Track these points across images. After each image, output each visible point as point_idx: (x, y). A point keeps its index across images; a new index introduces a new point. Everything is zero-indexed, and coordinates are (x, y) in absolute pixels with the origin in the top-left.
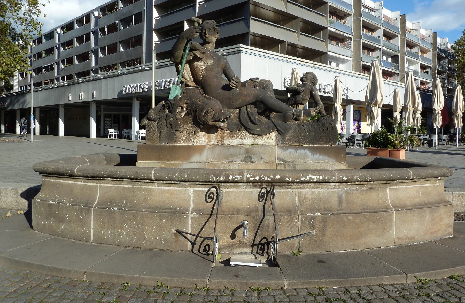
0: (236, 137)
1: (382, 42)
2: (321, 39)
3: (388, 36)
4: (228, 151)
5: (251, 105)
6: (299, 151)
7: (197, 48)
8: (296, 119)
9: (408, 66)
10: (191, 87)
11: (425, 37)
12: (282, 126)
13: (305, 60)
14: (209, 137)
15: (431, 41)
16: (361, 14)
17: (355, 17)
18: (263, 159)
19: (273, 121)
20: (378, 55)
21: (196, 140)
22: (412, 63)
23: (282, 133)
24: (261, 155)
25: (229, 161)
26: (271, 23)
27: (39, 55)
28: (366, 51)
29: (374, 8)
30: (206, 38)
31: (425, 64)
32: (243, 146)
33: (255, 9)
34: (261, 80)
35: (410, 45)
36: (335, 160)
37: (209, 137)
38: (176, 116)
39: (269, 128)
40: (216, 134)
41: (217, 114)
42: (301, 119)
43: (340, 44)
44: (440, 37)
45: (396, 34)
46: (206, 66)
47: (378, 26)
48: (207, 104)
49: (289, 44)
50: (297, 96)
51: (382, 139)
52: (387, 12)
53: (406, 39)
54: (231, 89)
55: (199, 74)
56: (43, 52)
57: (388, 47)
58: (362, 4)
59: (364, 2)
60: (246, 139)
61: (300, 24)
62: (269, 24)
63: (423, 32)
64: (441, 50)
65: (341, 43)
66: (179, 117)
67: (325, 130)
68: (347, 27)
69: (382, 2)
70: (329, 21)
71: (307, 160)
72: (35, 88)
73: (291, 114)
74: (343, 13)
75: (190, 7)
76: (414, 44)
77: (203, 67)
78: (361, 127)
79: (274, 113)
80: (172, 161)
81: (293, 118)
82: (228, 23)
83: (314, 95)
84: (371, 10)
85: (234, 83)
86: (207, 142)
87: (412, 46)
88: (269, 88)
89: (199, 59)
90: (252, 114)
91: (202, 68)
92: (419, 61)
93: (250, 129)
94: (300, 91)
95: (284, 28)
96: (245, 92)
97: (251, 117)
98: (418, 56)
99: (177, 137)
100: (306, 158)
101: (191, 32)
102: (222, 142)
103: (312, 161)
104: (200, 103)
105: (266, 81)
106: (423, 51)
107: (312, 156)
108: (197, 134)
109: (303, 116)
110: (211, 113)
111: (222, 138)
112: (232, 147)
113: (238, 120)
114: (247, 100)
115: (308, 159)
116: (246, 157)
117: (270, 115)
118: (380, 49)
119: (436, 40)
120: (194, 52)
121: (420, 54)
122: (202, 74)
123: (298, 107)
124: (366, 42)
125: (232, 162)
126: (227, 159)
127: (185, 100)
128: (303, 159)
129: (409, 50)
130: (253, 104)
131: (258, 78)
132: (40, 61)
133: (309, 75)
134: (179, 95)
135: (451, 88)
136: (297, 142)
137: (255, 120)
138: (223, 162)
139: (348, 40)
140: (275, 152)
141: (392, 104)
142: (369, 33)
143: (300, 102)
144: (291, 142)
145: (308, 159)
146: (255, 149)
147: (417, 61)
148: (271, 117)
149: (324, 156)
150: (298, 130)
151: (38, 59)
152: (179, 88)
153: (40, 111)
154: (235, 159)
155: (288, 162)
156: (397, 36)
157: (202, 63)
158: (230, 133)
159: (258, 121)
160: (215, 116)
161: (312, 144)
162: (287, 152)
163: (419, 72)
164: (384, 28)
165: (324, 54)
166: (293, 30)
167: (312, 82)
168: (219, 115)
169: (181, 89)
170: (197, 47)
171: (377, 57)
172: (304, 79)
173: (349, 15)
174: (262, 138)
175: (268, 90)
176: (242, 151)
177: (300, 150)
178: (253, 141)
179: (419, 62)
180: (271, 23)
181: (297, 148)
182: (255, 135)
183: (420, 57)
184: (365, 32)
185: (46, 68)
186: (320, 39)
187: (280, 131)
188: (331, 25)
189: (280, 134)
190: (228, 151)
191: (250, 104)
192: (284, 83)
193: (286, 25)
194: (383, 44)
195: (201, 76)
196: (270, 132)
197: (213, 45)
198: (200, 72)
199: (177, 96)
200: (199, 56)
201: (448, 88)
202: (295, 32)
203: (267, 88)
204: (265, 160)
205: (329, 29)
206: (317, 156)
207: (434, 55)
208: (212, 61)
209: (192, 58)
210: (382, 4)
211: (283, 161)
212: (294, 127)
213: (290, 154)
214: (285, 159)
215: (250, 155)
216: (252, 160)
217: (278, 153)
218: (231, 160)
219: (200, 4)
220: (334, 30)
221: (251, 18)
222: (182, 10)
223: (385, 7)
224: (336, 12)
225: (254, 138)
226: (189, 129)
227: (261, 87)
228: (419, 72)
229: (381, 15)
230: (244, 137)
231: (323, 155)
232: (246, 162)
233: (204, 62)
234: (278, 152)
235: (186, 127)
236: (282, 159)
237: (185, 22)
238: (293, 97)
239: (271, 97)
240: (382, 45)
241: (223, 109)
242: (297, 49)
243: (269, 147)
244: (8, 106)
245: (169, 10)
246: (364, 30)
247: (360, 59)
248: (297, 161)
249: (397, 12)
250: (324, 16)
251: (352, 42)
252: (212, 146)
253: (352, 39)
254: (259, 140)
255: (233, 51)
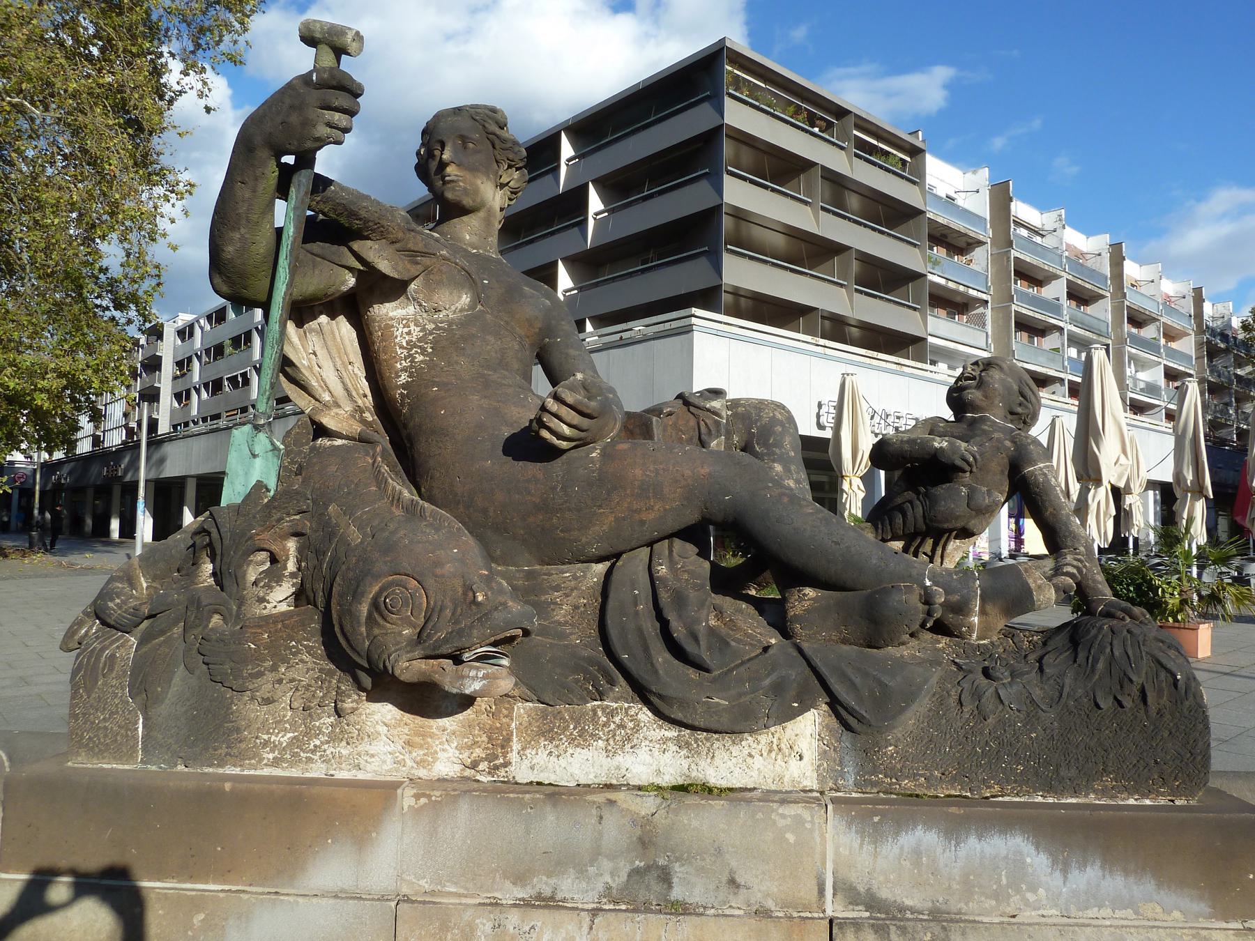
0: (583, 738)
1: (1065, 312)
2: (910, 304)
3: (1079, 296)
4: (528, 832)
5: (678, 544)
6: (973, 841)
7: (366, 221)
8: (941, 628)
9: (1133, 372)
10: (339, 442)
11: (1173, 299)
12: (858, 681)
13: (874, 354)
14: (418, 734)
15: (1190, 310)
16: (1011, 242)
17: (995, 248)
18: (743, 891)
19: (805, 646)
20: (1057, 345)
21: (344, 752)
22: (1143, 366)
23: (860, 719)
24: (734, 864)
25: (533, 893)
26: (779, 262)
27: (219, 351)
28: (1025, 335)
29: (1040, 227)
30: (445, 183)
31: (1175, 366)
32: (619, 796)
33: (737, 228)
34: (735, 404)
35: (1138, 320)
36: (1203, 907)
37: (424, 736)
38: (241, 602)
39: (778, 689)
40: (460, 716)
41: (448, 612)
42: (970, 628)
43: (957, 317)
44: (1210, 300)
45: (1101, 292)
46: (430, 326)
47: (1054, 271)
48: (389, 548)
49: (825, 315)
50: (940, 490)
51: (1132, 589)
52: (1074, 238)
53: (1126, 303)
54: (551, 453)
55: (392, 367)
56: (228, 342)
57: (1082, 323)
58: (1012, 218)
59: (1016, 212)
60: (643, 753)
61: (855, 266)
62: (774, 265)
63: (1169, 287)
64: (1213, 332)
65: (961, 313)
66: (258, 611)
67: (1127, 703)
68: (976, 273)
69: (1063, 211)
70: (930, 258)
71: (1027, 903)
72: (206, 424)
73: (914, 600)
74: (964, 239)
75: (573, 225)
76: (1145, 317)
77: (416, 332)
78: (1023, 533)
79: (810, 592)
80: (191, 878)
81: (923, 626)
82: (667, 264)
83: (1037, 484)
84: (1036, 232)
85: (568, 419)
86: (409, 763)
87: (1140, 321)
88: (778, 444)
89: (395, 289)
90: (680, 600)
91: (409, 333)
92: (1160, 360)
93: (660, 697)
94: (959, 462)
95: (812, 276)
96: (638, 472)
97: (671, 616)
98: (1159, 347)
99: (238, 730)
100: (1018, 891)
101: (292, 107)
102: (497, 768)
103: (1056, 906)
104: (355, 536)
105: (761, 405)
106: (1171, 335)
107: (1058, 874)
108: (352, 718)
109: (983, 612)
110: (405, 604)
111: (499, 743)
112: (548, 808)
113: (594, 632)
114: (650, 516)
115: (1031, 897)
116: (636, 872)
117: (784, 600)
118: (1061, 329)
119: (1203, 307)
120: (356, 245)
121: (1163, 341)
122: (404, 370)
123: (939, 552)
124: (1024, 311)
125: (552, 898)
126: (520, 879)
127: (288, 514)
128: (999, 896)
129: (1134, 331)
130: (693, 534)
131: (717, 393)
132: (221, 363)
133: (995, 374)
134: (272, 483)
135: (1245, 427)
136: (954, 779)
137: (695, 637)
138: (496, 904)
139: (978, 307)
140: (818, 849)
141: (1172, 481)
142: (1031, 290)
143: (959, 524)
144: (914, 777)
145: (1031, 897)
146: (695, 823)
147: (1156, 359)
148: (791, 613)
149: (1131, 879)
150: (960, 703)
151: (215, 359)
152: (270, 447)
153: (198, 485)
154: (568, 886)
155: (902, 909)
156: (1103, 297)
157: (411, 310)
158: (544, 716)
159: (709, 648)
160: (430, 624)
161: (1049, 789)
162: (896, 850)
163: (1163, 387)
164: (1070, 278)
165: (917, 341)
166: (835, 280)
167: (1012, 413)
168: (457, 622)
169: (275, 448)
170: (363, 213)
171: (1054, 349)
172: (973, 395)
173: (980, 243)
174: (735, 750)
175: (774, 453)
176: (614, 831)
177: (980, 837)
178: (685, 763)
179: (1160, 363)
180: (779, 262)
181: (954, 830)
182: (693, 728)
183: (1162, 350)
184: (1020, 286)
185: (233, 380)
186: (907, 303)
187: (851, 712)
188: (933, 269)
189: (847, 726)
190: (528, 832)
191: (669, 536)
192: (818, 416)
193: (818, 268)
194: (1067, 317)
195: (404, 378)
196: (791, 715)
197: (488, 221)
198: (395, 358)
199: (260, 486)
200: (384, 266)
201: (1238, 428)
202: (841, 285)
203: (765, 444)
204: (757, 897)
205: (930, 277)
206: (1088, 876)
207: (1199, 345)
208: (465, 299)
209: (352, 281)
210: (1063, 216)
211: (872, 902)
212: (934, 680)
213: (917, 863)
214: (884, 894)
215: (661, 862)
216: (677, 893)
217: (837, 853)
218: (547, 892)
219: (598, 217)
220: (942, 282)
221: (728, 250)
222: (552, 233)
223: (1069, 226)
224: (946, 238)
225: (688, 744)
226: (307, 687)
227: (736, 438)
228: (1163, 387)
229: (1062, 244)
230: (627, 739)
231: (1126, 873)
232: (641, 908)
233: (420, 305)
234: (837, 848)
235: (290, 675)
236: (861, 889)
237: (560, 264)
238: (909, 495)
239: (794, 499)
240: (1067, 318)
241: (488, 580)
242: (847, 329)
243: (783, 816)
244: (126, 471)
245: (522, 235)
246: (1019, 282)
247: (1011, 355)
248: (962, 905)
249: (1099, 237)
250: (915, 245)
251: (989, 312)
252: (429, 797)
253: (989, 304)
254: (717, 761)
255: (672, 327)
